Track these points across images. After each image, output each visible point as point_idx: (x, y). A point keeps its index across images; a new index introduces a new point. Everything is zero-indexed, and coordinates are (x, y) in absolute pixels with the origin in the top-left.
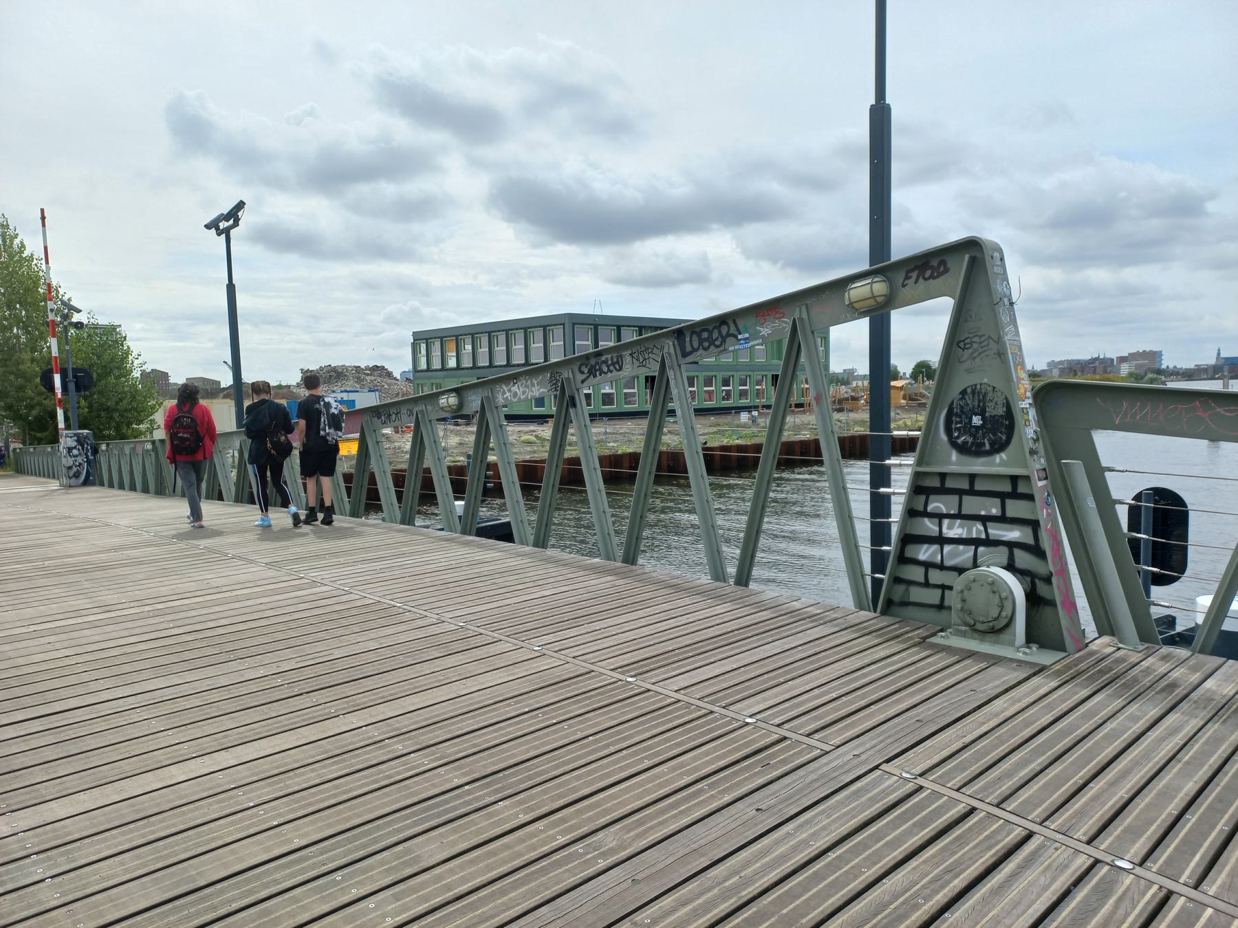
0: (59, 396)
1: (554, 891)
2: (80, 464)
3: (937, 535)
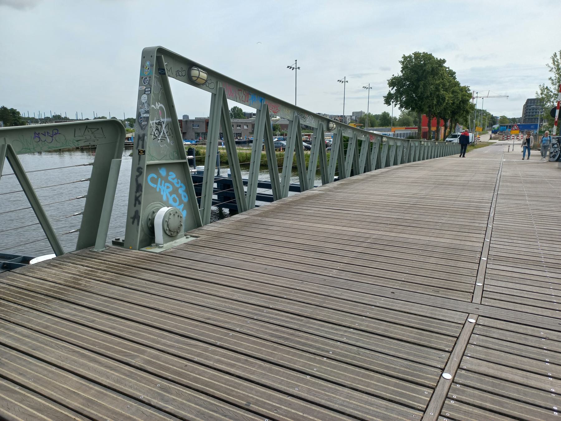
0: (556, 120)
1: (72, 368)
2: (557, 152)
3: (92, 166)
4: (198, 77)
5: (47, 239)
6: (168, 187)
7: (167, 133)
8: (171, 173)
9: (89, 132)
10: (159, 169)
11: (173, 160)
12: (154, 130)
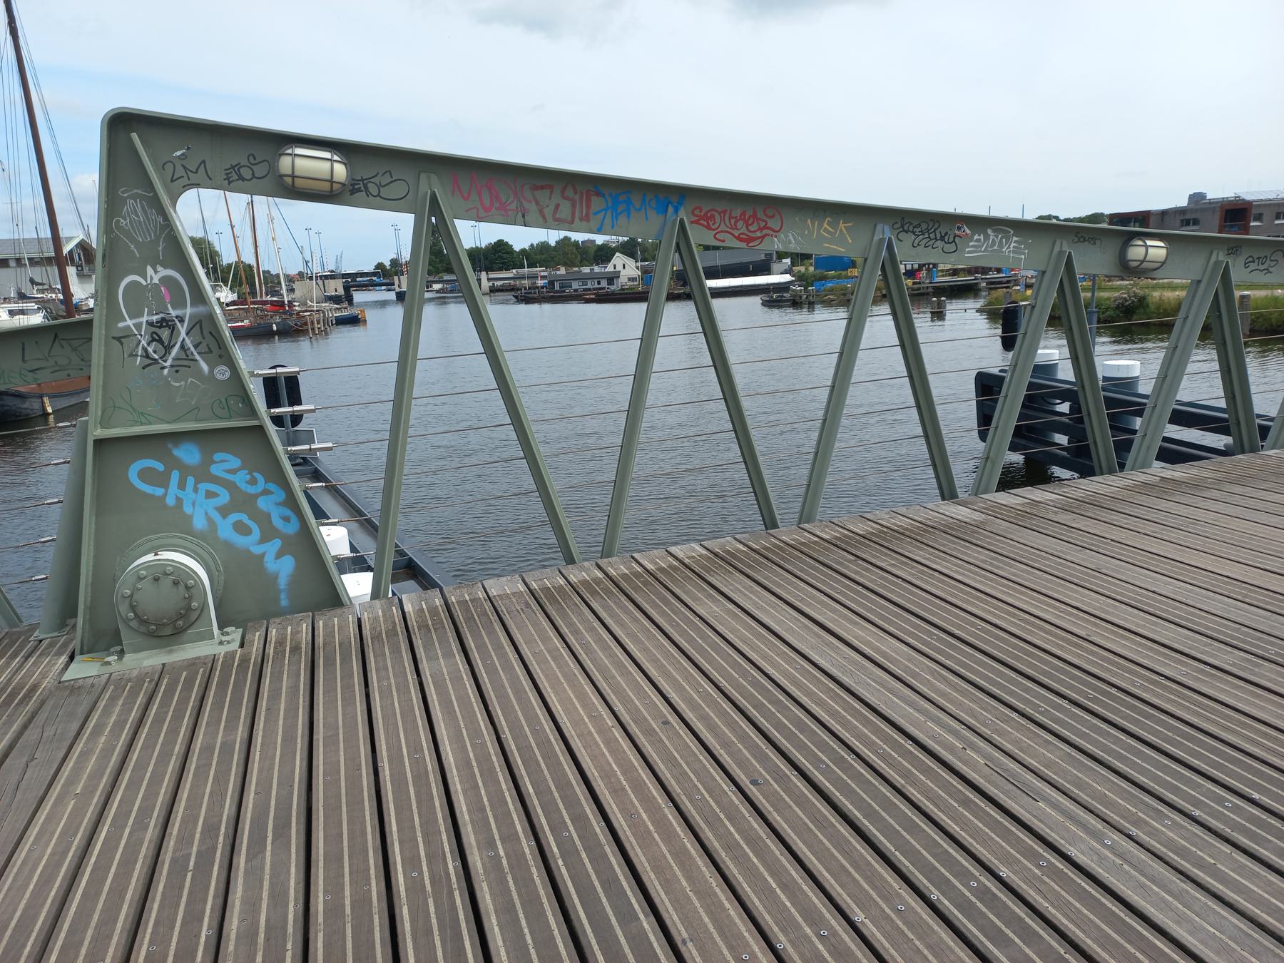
4: (293, 176)
5: (753, 494)
6: (210, 495)
7: (196, 347)
8: (218, 456)
9: (62, 347)
10: (170, 446)
11: (230, 418)
12: (144, 343)
